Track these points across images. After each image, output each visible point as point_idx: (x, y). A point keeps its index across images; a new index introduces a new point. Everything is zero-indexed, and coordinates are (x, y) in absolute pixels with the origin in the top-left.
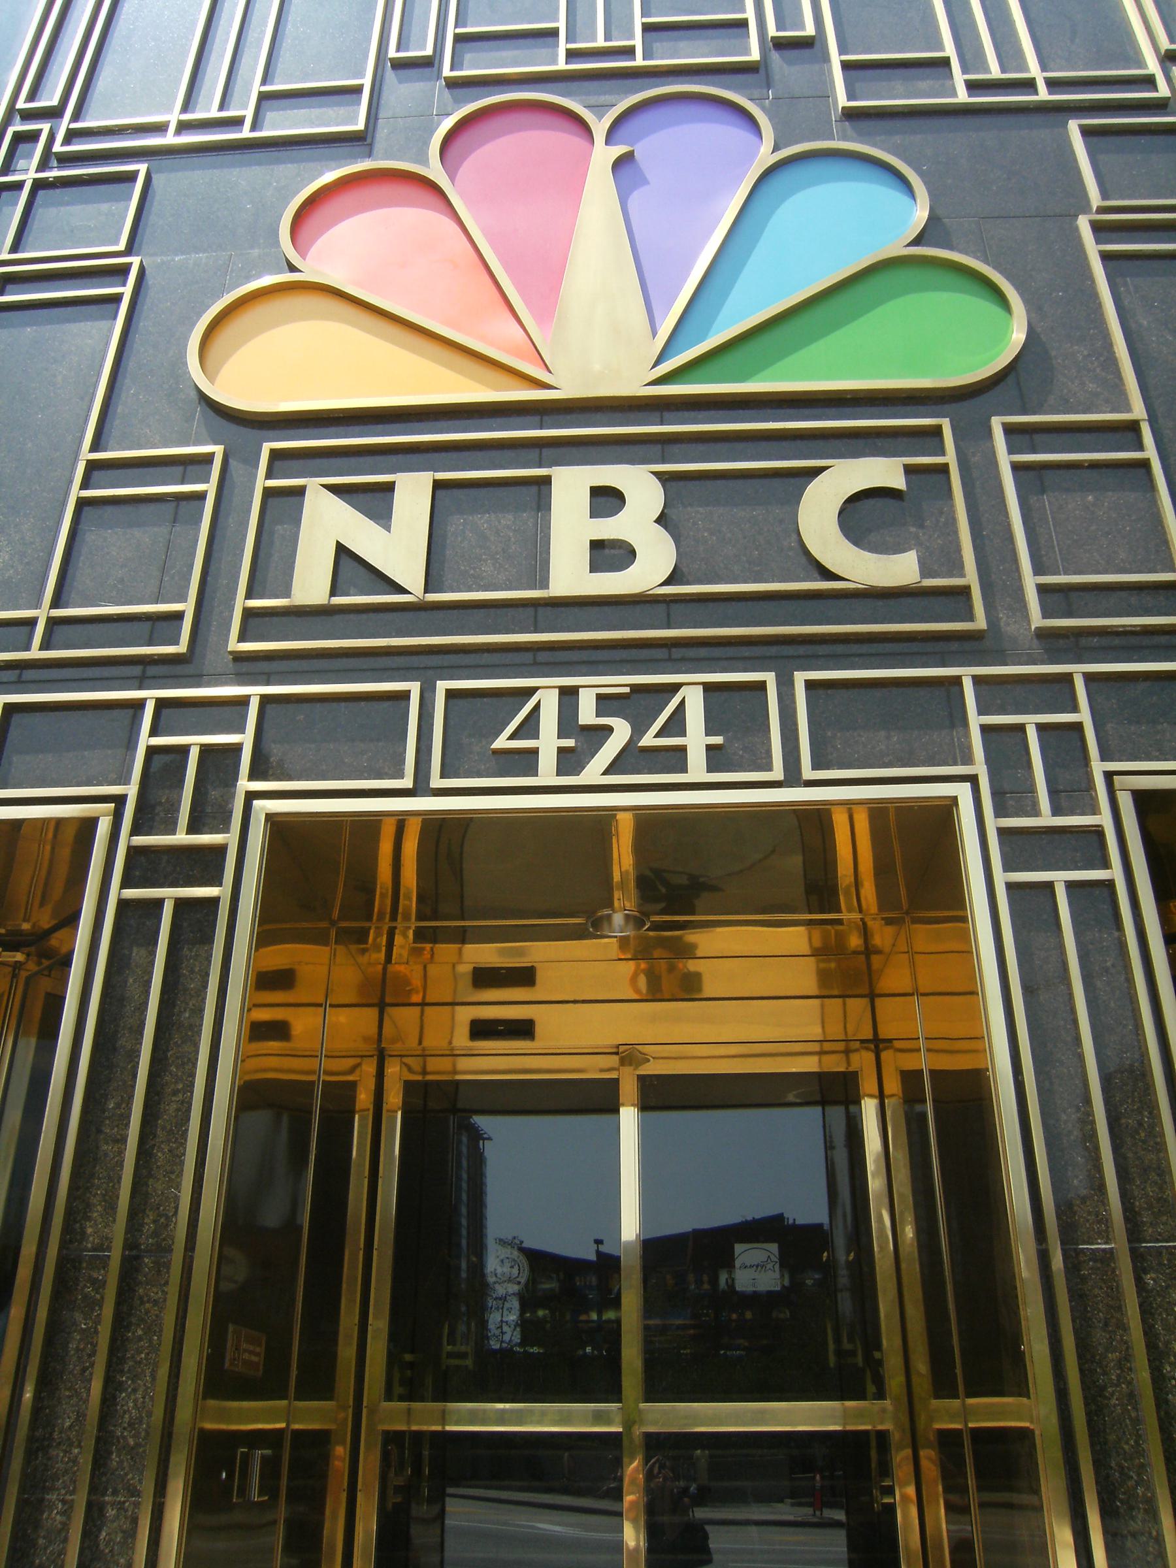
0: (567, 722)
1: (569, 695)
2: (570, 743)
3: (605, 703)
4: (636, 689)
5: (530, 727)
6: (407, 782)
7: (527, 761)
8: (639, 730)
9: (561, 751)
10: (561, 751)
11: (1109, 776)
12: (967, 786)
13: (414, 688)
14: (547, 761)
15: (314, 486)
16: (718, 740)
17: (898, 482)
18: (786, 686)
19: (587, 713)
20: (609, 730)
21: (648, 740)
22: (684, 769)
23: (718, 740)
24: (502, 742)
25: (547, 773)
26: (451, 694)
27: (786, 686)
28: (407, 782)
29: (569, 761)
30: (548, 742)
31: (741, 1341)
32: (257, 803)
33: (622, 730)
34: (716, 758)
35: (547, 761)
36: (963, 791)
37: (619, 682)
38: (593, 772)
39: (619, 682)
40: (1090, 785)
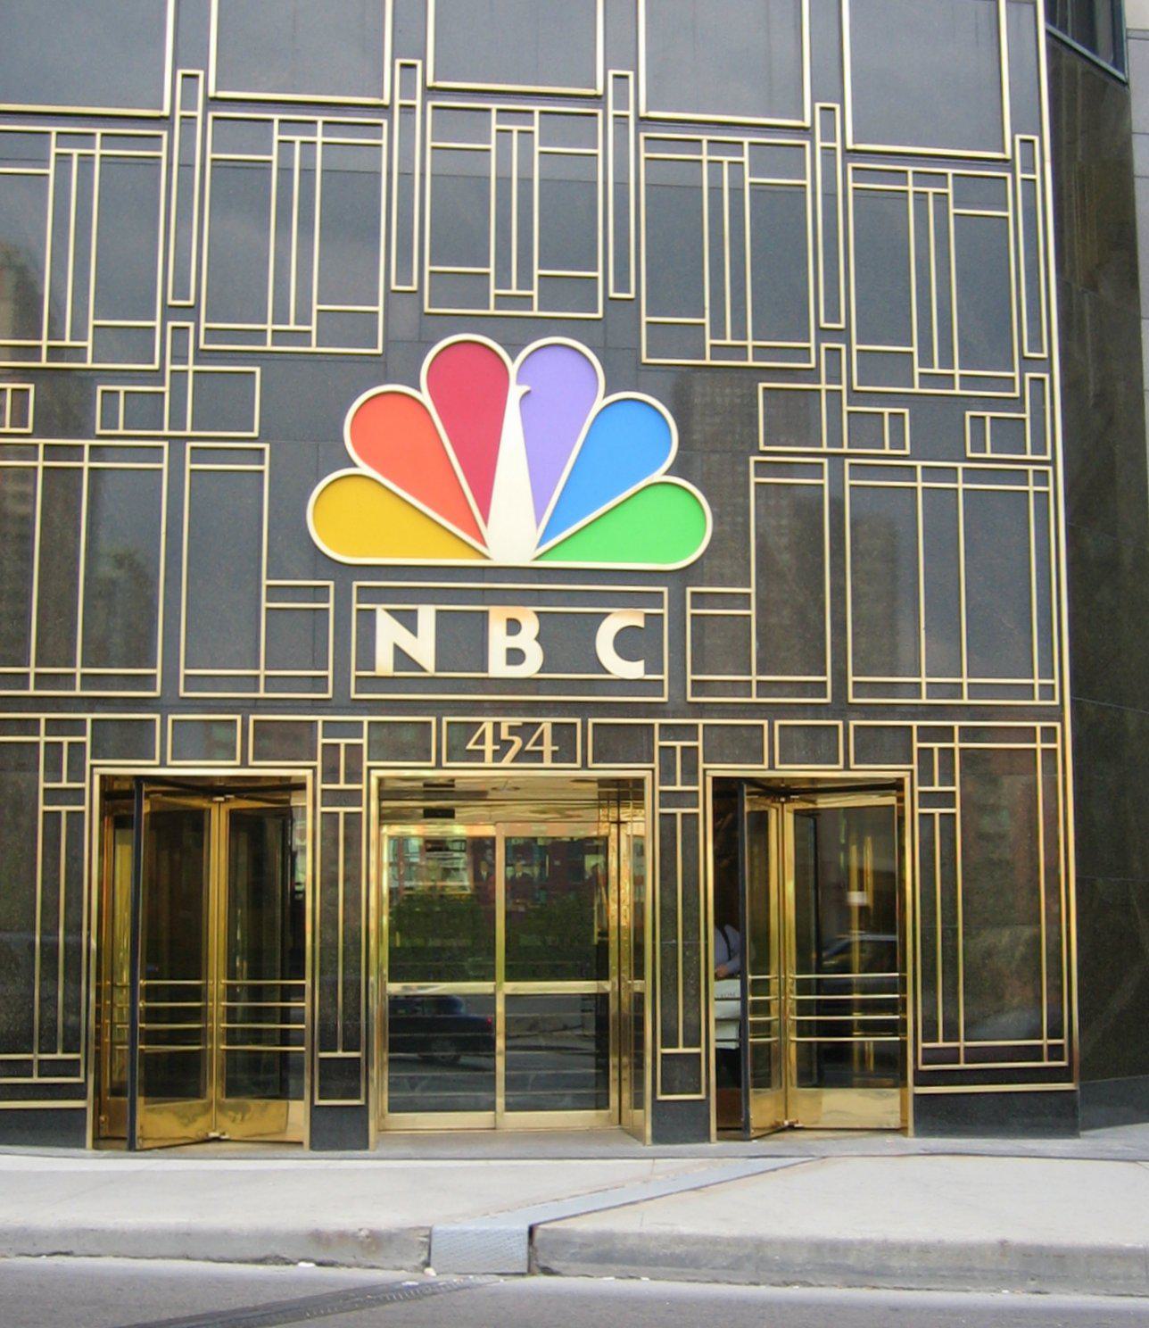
0: (497, 739)
1: (497, 725)
2: (498, 747)
3: (513, 730)
4: (525, 724)
5: (481, 740)
6: (157, 762)
7: (480, 755)
8: (525, 744)
9: (495, 751)
10: (495, 751)
11: (705, 770)
12: (650, 772)
13: (433, 720)
14: (489, 755)
15: (380, 610)
16: (556, 748)
17: (641, 623)
18: (164, 722)
19: (504, 735)
20: (512, 742)
21: (529, 747)
22: (483, 761)
23: (556, 748)
24: (470, 746)
25: (488, 762)
26: (174, 721)
27: (164, 722)
28: (157, 762)
29: (498, 756)
30: (489, 747)
31: (238, 964)
32: (96, 770)
33: (518, 741)
34: (556, 757)
35: (489, 755)
36: (98, 771)
37: (517, 721)
38: (506, 762)
39: (517, 721)
40: (697, 772)
